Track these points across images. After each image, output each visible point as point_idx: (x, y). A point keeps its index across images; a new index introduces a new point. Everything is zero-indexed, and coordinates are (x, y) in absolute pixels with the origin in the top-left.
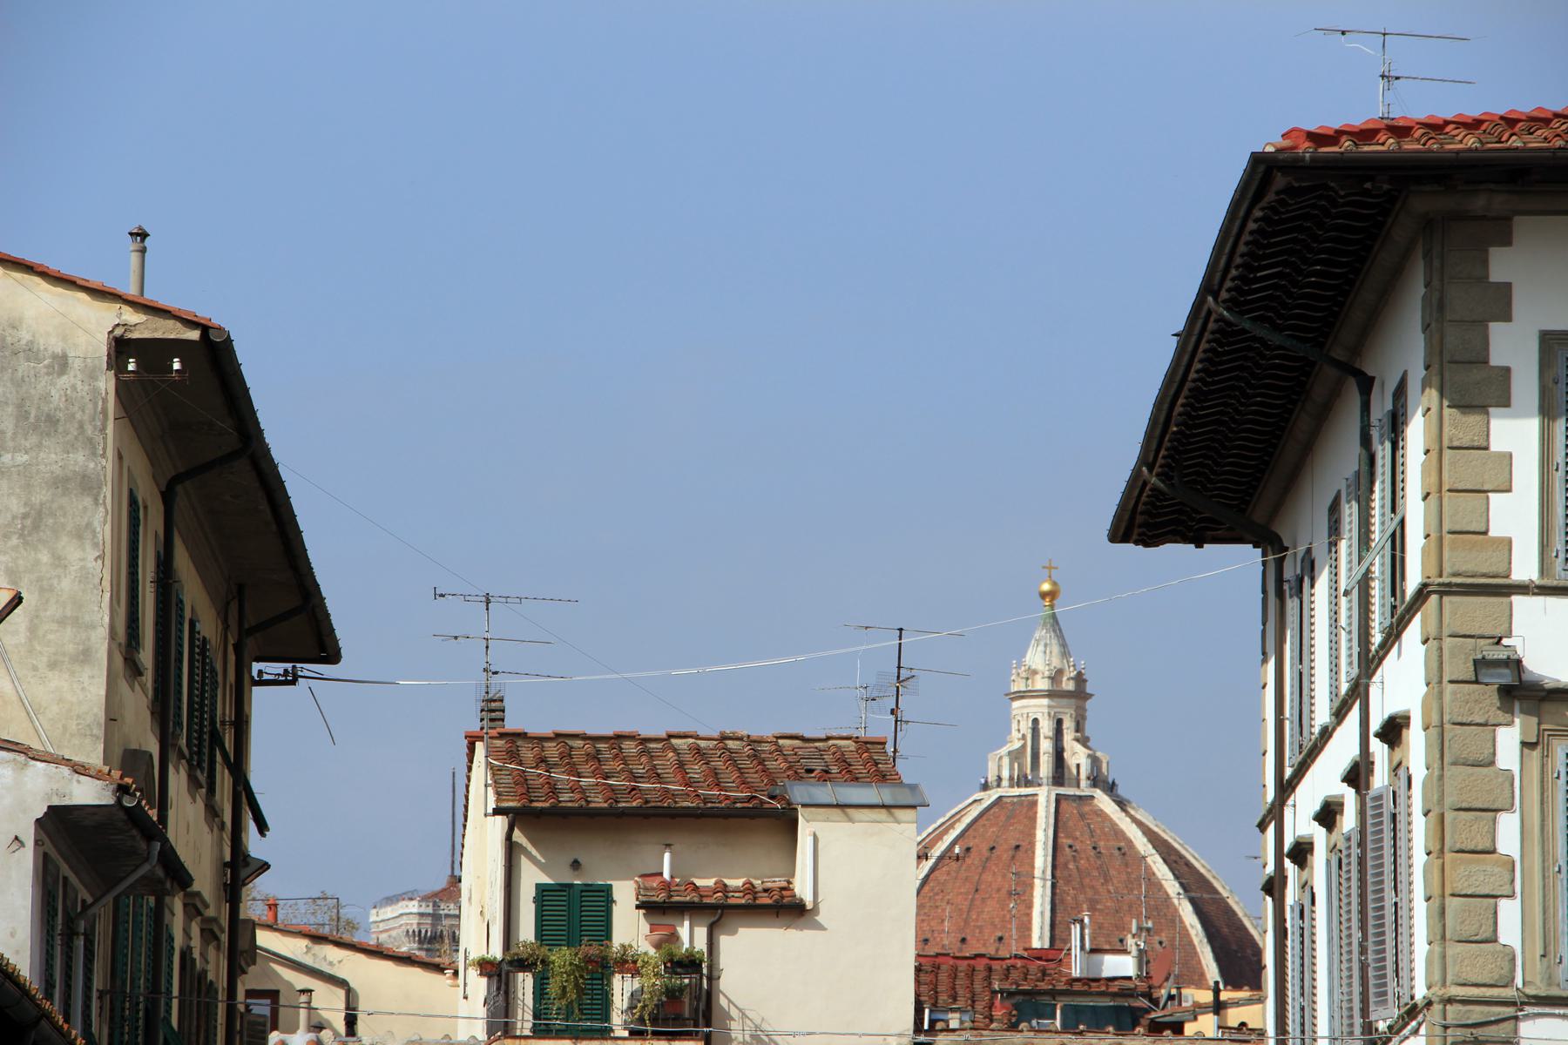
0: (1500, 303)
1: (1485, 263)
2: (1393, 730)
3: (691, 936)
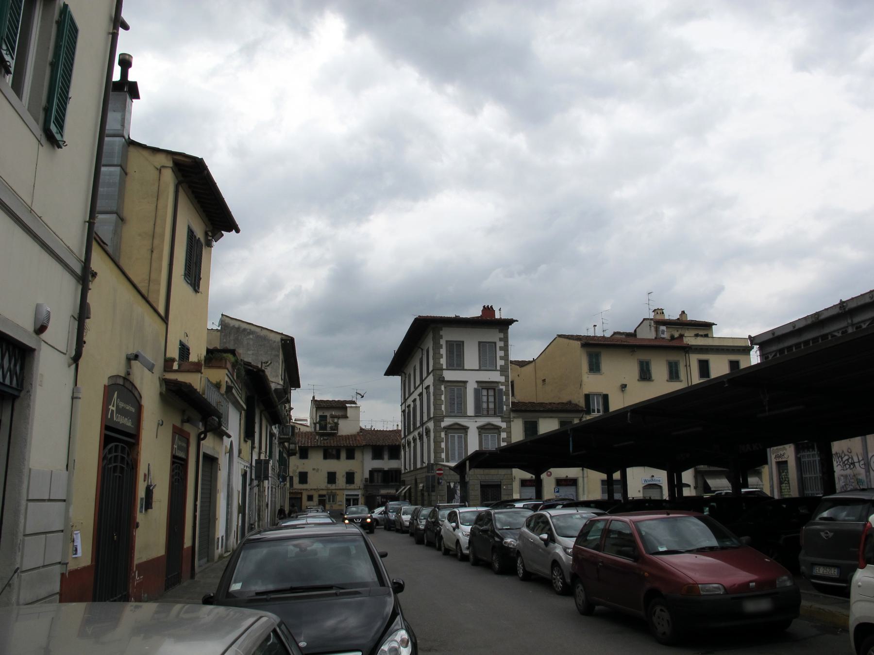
0: (441, 337)
1: (439, 332)
2: (428, 387)
3: (336, 420)
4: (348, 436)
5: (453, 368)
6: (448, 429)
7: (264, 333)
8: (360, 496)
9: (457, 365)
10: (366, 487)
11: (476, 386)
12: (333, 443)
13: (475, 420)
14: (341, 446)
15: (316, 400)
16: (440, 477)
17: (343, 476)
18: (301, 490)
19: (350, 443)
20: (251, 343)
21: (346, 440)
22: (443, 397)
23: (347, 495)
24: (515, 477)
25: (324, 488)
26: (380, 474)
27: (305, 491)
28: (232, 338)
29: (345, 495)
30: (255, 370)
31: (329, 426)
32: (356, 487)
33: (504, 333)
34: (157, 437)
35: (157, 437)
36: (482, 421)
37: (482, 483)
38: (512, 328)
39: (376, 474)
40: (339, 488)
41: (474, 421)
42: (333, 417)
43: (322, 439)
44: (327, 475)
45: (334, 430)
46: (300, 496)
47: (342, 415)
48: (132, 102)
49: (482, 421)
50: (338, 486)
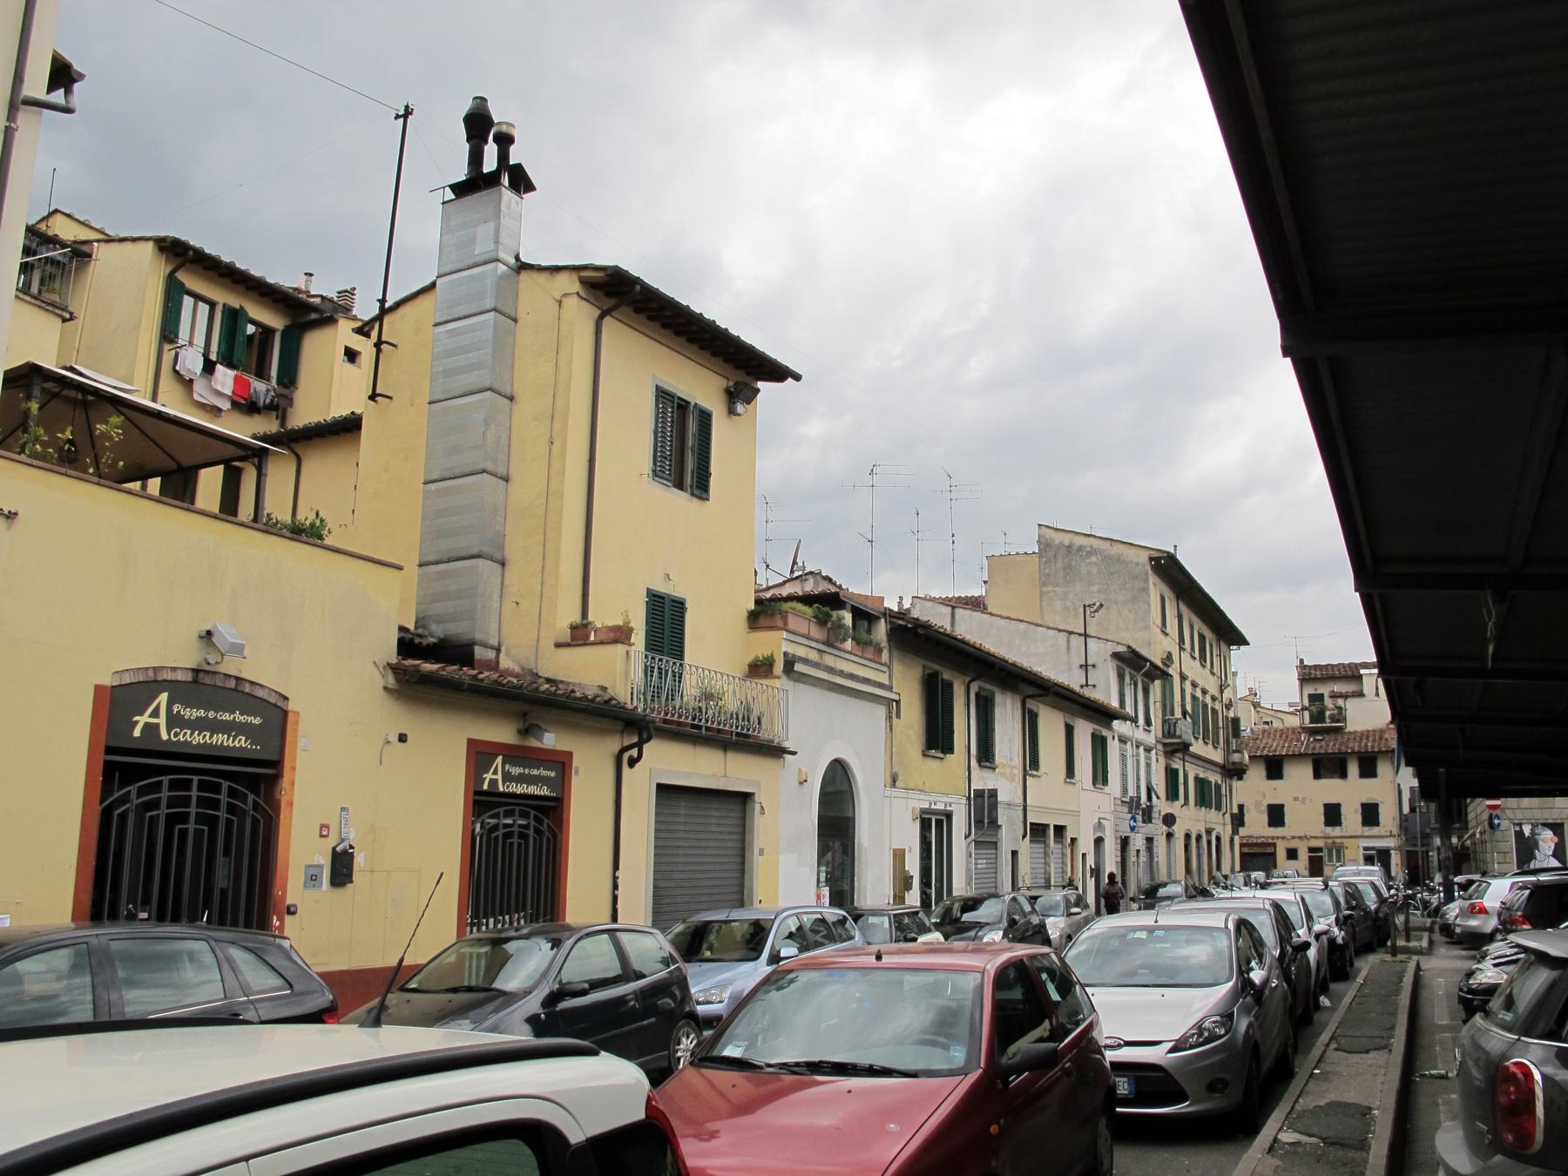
3: (1340, 702)
7: (1117, 549)
12: (1331, 746)
14: (1347, 753)
15: (1306, 666)
16: (1497, 812)
17: (1356, 812)
18: (1273, 838)
19: (1366, 746)
20: (1094, 571)
21: (1361, 740)
23: (1366, 849)
25: (1318, 835)
27: (1280, 840)
28: (1060, 565)
29: (1361, 849)
30: (910, 626)
32: (1383, 833)
34: (381, 763)
35: (381, 763)
40: (1348, 835)
42: (1334, 696)
43: (1312, 739)
44: (1322, 810)
45: (1338, 721)
46: (1273, 850)
47: (1353, 692)
48: (522, 198)
50: (1346, 831)
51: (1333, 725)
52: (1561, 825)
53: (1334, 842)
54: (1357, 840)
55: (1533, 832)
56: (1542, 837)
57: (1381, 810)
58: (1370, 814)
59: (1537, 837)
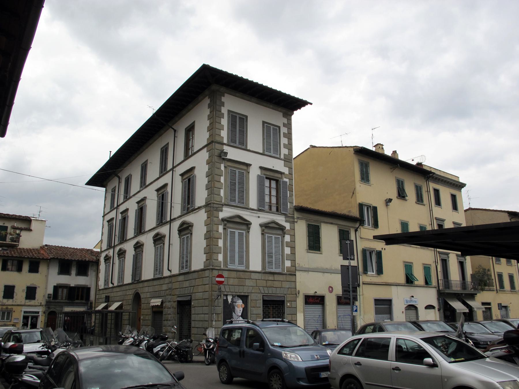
0: (223, 104)
3: (18, 232)
4: (30, 249)
5: (235, 145)
6: (227, 221)
8: (40, 314)
9: (240, 143)
10: (48, 304)
11: (259, 172)
13: (258, 215)
14: (24, 258)
17: (23, 291)
22: (222, 179)
23: (25, 312)
24: (299, 291)
26: (65, 291)
31: (9, 237)
32: (37, 304)
33: (288, 119)
36: (266, 218)
37: (266, 298)
38: (298, 116)
39: (60, 290)
40: (16, 304)
41: (256, 217)
42: (14, 228)
44: (3, 289)
45: (15, 241)
47: (25, 228)
49: (266, 218)
51: (13, 243)
52: (247, 297)
53: (7, 308)
54: (21, 307)
55: (232, 301)
56: (237, 304)
57: (38, 291)
58: (31, 292)
59: (234, 304)
